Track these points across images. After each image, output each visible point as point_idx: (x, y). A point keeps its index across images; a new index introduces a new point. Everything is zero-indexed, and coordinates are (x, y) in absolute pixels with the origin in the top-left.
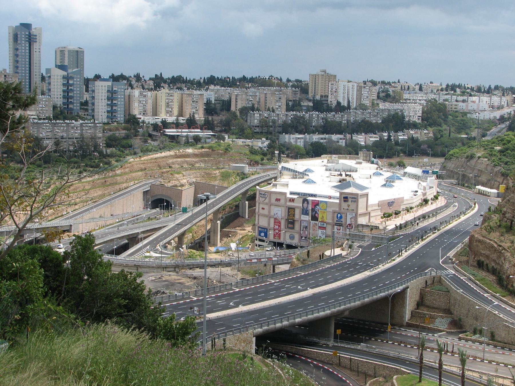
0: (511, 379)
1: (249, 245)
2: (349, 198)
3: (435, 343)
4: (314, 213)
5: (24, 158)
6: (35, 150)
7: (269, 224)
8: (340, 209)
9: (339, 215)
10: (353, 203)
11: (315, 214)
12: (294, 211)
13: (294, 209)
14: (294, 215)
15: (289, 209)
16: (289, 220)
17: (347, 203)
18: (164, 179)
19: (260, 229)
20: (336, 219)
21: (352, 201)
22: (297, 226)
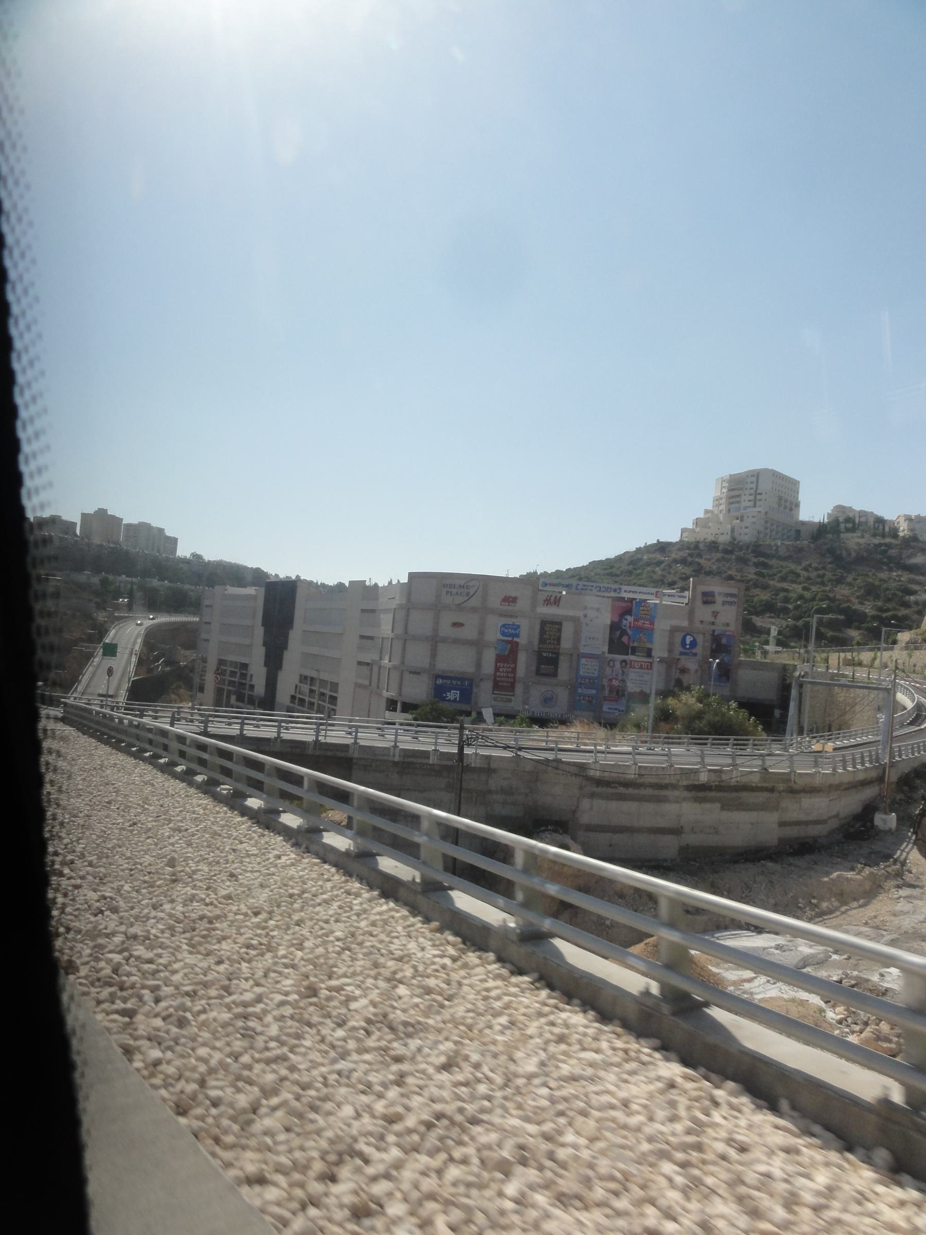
0: (285, 1190)
1: (127, 985)
2: (716, 595)
3: (248, 989)
4: (618, 633)
5: (241, 740)
6: (155, 590)
7: (478, 665)
8: (691, 619)
9: (689, 639)
10: (727, 606)
11: (621, 636)
12: (560, 630)
13: (560, 624)
14: (558, 640)
15: (544, 623)
16: (545, 655)
17: (710, 609)
18: (194, 812)
19: (440, 681)
20: (678, 648)
21: (725, 603)
22: (564, 672)
